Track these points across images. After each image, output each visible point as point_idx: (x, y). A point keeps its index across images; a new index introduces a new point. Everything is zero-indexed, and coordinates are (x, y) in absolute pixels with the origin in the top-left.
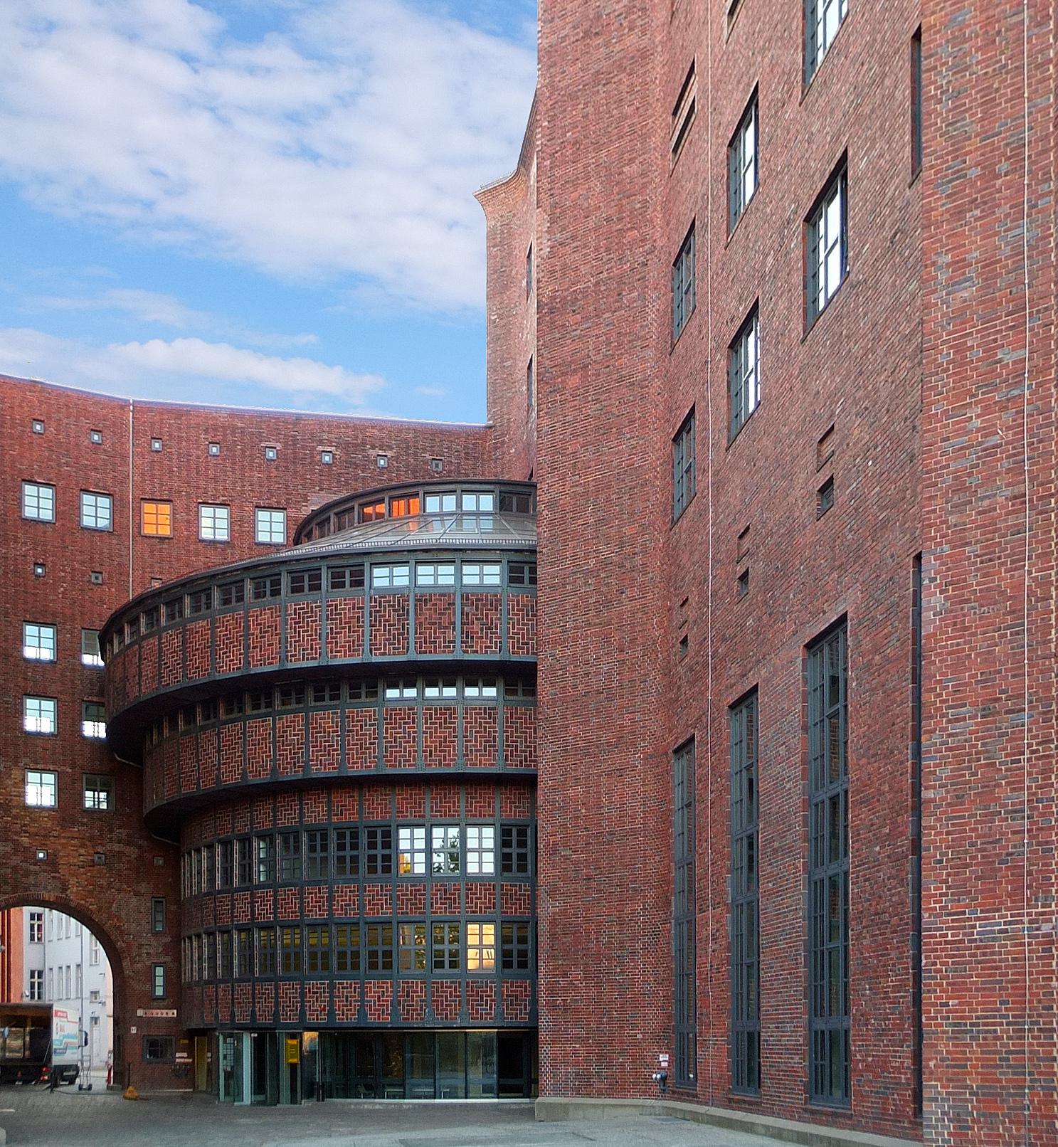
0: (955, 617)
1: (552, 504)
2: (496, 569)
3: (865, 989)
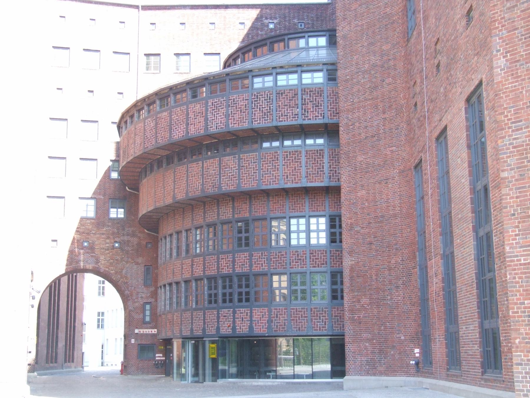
0: (512, 71)
1: (344, 37)
2: (320, 74)
3: (504, 301)
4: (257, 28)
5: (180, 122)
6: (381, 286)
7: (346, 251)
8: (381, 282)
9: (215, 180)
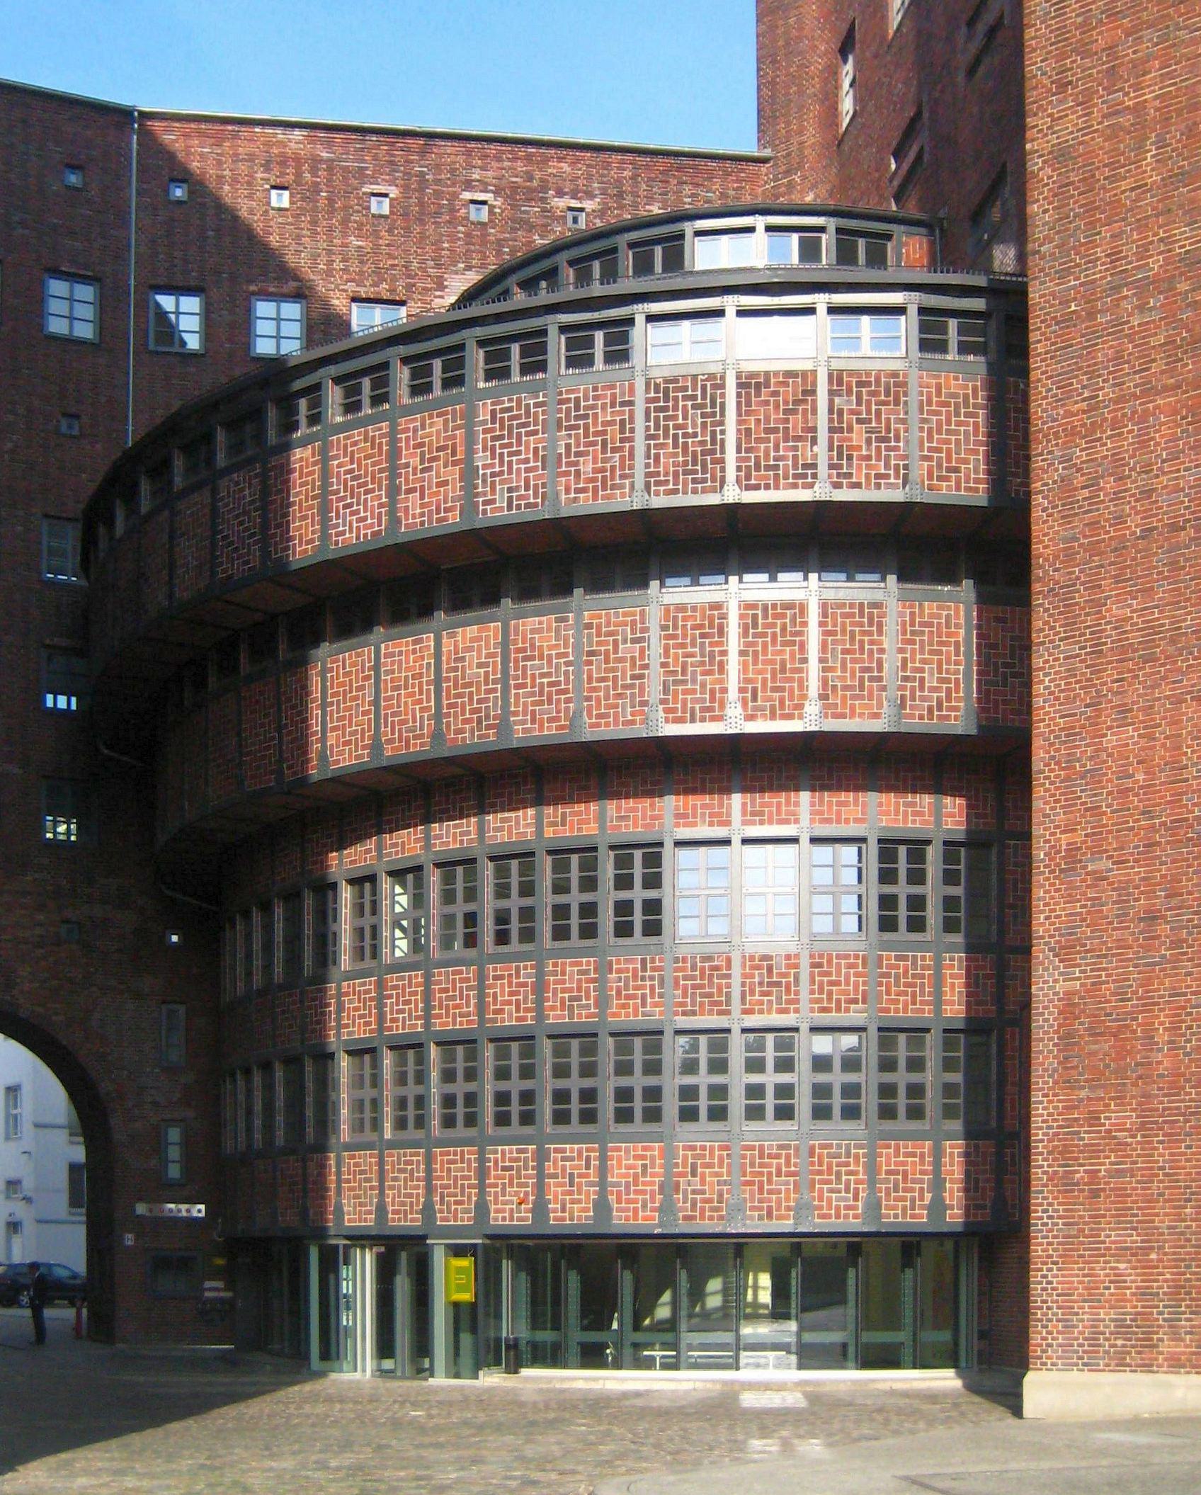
1: (1060, 156)
4: (527, 222)
5: (366, 484)
6: (1188, 1067)
7: (1046, 944)
8: (1188, 1054)
9: (486, 700)
